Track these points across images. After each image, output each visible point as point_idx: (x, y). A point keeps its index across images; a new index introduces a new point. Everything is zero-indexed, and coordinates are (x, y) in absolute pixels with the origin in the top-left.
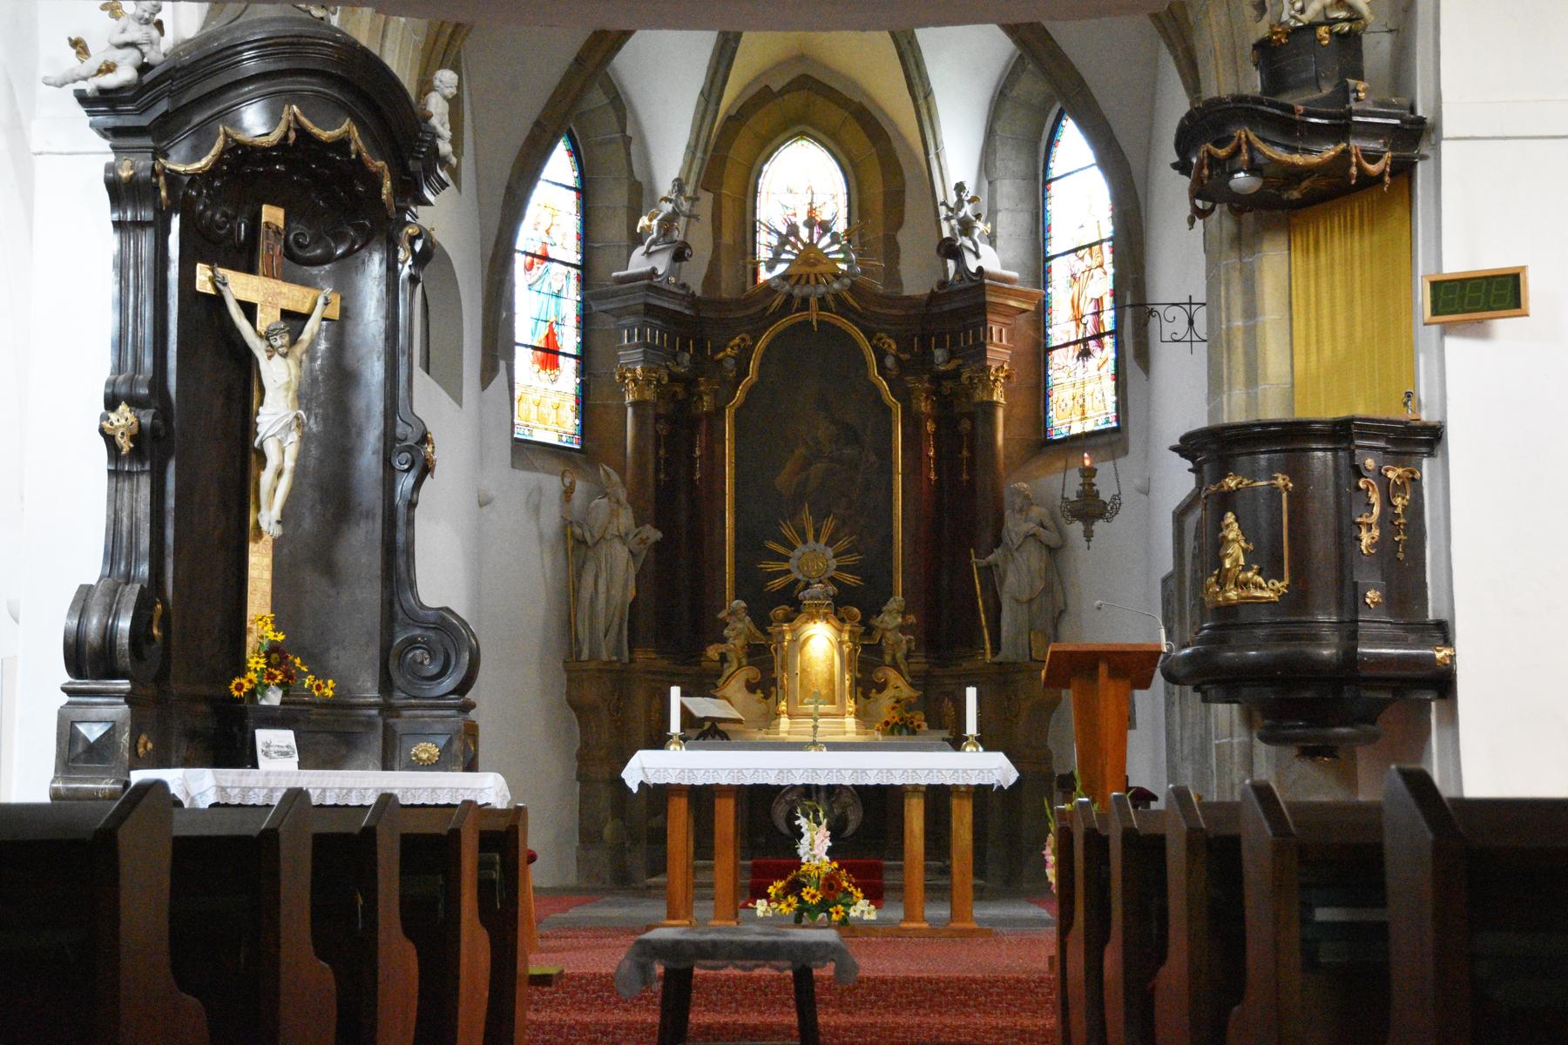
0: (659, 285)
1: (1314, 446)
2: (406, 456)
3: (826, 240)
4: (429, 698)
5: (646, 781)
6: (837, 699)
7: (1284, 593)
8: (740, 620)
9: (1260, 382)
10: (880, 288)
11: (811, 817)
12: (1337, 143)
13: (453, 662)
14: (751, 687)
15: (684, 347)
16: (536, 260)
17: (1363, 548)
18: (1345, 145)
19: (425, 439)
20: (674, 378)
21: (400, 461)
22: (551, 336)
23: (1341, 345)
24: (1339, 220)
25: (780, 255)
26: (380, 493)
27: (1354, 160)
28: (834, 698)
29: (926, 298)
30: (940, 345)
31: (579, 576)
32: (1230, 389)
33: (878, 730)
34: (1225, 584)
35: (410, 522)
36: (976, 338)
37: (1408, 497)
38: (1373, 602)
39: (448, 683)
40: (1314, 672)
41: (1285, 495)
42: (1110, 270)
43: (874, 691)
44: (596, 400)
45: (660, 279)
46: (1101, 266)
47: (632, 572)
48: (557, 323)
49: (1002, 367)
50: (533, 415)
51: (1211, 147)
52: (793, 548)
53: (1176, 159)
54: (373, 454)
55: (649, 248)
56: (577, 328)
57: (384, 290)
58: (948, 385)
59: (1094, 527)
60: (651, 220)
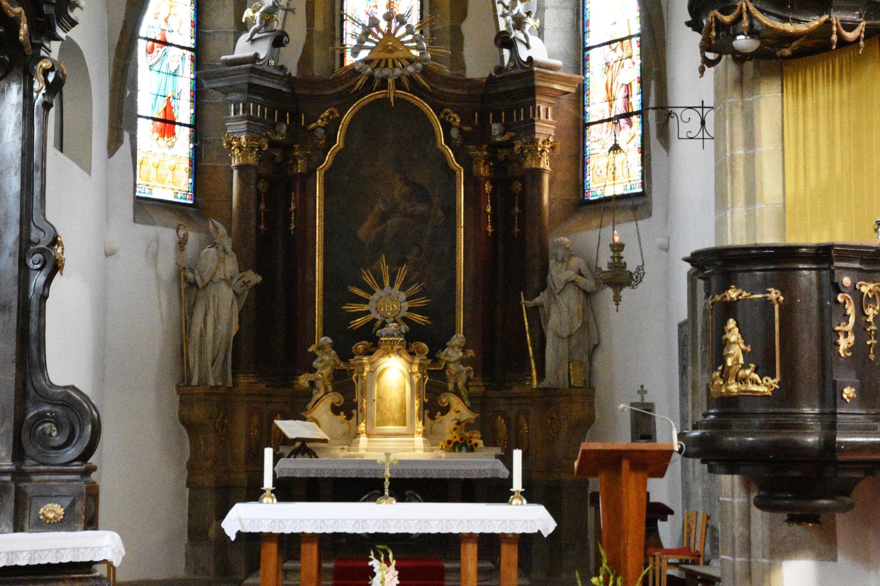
0: (260, 68)
1: (801, 266)
2: (38, 257)
3: (403, 30)
4: (56, 465)
5: (243, 530)
6: (408, 421)
7: (776, 389)
8: (327, 354)
9: (758, 202)
10: (447, 71)
11: (382, 558)
12: (821, 15)
13: (77, 435)
14: (335, 410)
15: (282, 119)
16: (156, 44)
17: (841, 351)
18: (827, 16)
19: (55, 241)
20: (272, 144)
21: (34, 261)
22: (168, 109)
23: (824, 174)
24: (823, 68)
25: (364, 42)
26: (16, 288)
27: (835, 29)
28: (405, 420)
29: (484, 81)
30: (497, 119)
31: (190, 313)
32: (733, 207)
33: (442, 449)
34: (727, 379)
35: (42, 313)
36: (527, 114)
37: (878, 308)
38: (848, 397)
39: (72, 452)
40: (800, 453)
41: (777, 307)
42: (638, 61)
43: (439, 413)
44: (206, 163)
45: (261, 63)
46: (630, 57)
47: (236, 310)
48: (174, 98)
49: (548, 140)
50: (153, 175)
51: (718, 13)
52: (372, 292)
53: (689, 18)
54: (10, 255)
55: (253, 35)
56: (191, 101)
57: (21, 115)
58: (502, 154)
59: (622, 293)
60: (254, 12)
